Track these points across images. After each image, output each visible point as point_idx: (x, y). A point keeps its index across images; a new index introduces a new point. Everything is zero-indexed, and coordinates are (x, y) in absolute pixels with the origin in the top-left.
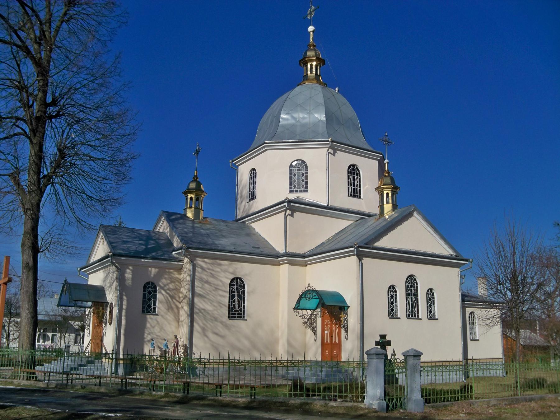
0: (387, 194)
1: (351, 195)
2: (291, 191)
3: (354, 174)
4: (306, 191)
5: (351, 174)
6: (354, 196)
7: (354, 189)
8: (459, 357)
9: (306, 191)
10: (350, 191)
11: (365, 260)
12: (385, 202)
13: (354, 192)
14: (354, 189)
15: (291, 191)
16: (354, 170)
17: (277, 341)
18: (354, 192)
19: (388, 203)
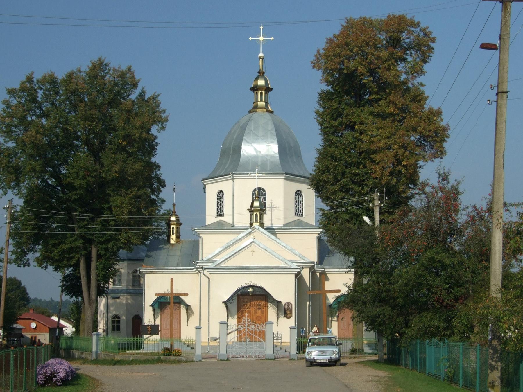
12: (171, 234)
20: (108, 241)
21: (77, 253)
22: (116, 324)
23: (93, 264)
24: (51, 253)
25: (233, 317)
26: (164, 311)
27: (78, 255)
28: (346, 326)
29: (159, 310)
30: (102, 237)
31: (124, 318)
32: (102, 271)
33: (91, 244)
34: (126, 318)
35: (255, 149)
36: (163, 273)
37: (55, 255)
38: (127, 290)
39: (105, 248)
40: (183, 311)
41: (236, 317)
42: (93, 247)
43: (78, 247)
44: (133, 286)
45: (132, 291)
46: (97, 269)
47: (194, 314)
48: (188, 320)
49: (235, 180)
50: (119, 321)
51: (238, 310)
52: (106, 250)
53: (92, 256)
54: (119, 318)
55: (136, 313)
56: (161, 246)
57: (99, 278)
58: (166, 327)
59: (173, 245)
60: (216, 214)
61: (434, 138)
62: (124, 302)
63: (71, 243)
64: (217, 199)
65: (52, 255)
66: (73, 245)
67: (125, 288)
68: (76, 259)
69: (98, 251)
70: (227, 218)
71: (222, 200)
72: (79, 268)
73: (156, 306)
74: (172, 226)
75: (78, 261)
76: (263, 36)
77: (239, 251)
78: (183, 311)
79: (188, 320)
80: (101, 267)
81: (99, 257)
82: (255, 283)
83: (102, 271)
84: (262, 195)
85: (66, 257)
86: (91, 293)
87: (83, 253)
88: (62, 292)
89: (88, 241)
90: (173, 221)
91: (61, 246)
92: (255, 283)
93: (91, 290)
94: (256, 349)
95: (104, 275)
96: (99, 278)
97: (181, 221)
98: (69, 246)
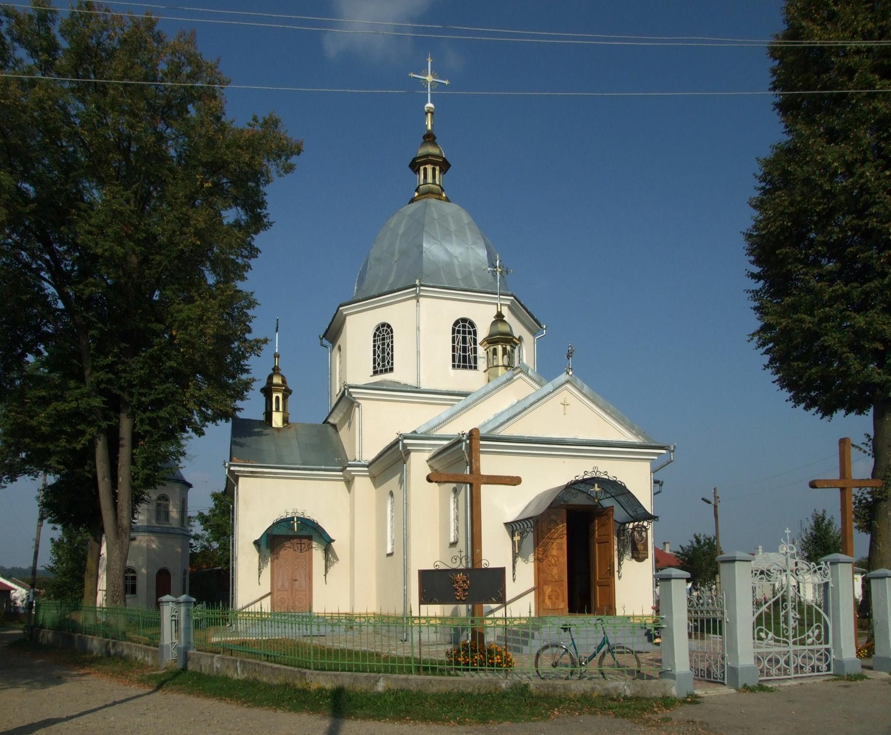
0: (277, 398)
1: (459, 366)
2: (475, 368)
3: (464, 332)
4: (391, 370)
5: (459, 332)
6: (464, 367)
7: (464, 357)
8: (835, 475)
9: (391, 370)
10: (457, 360)
11: (400, 611)
12: (274, 409)
13: (465, 361)
14: (464, 357)
15: (475, 368)
16: (464, 326)
17: (440, 172)
18: (465, 361)
19: (277, 410)
20: (158, 404)
21: (91, 424)
22: (130, 583)
23: (124, 454)
24: (32, 418)
25: (526, 560)
26: (277, 553)
27: (92, 430)
28: (287, 585)
29: (269, 551)
30: (145, 395)
31: (144, 571)
32: (143, 467)
33: (118, 411)
34: (148, 572)
35: (447, 252)
36: (275, 476)
37: (41, 423)
38: (148, 526)
39: (150, 419)
40: (318, 555)
41: (531, 558)
42: (123, 416)
43: (91, 410)
44: (157, 520)
45: (156, 529)
46: (133, 462)
47: (337, 560)
48: (326, 571)
49: (421, 299)
50: (134, 578)
51: (536, 544)
52: (153, 422)
53: (121, 435)
54: (134, 572)
55: (162, 566)
56: (257, 430)
57: (137, 483)
58: (283, 586)
59: (278, 429)
60: (372, 370)
61: (57, 545)
62: (145, 545)
63: (77, 400)
64: (374, 341)
65: (34, 423)
66: (83, 404)
67: (145, 524)
68: (88, 437)
69: (134, 426)
70: (401, 373)
71: (387, 341)
72: (94, 459)
73: (263, 544)
74: (274, 395)
75: (92, 444)
76: (426, 75)
77: (531, 405)
78: (318, 555)
79: (326, 571)
80: (140, 461)
81: (136, 438)
82: (606, 473)
83: (143, 467)
84: (470, 333)
85: (65, 433)
86: (120, 514)
87: (104, 424)
88: (42, 519)
89: (115, 405)
90: (278, 385)
91: (54, 404)
92: (606, 473)
93: (119, 508)
94: (812, 644)
95: (149, 476)
96: (137, 483)
97: (290, 386)
98: (74, 404)
